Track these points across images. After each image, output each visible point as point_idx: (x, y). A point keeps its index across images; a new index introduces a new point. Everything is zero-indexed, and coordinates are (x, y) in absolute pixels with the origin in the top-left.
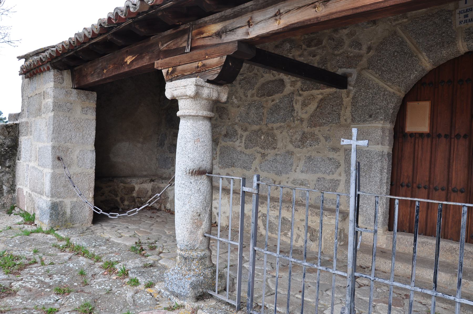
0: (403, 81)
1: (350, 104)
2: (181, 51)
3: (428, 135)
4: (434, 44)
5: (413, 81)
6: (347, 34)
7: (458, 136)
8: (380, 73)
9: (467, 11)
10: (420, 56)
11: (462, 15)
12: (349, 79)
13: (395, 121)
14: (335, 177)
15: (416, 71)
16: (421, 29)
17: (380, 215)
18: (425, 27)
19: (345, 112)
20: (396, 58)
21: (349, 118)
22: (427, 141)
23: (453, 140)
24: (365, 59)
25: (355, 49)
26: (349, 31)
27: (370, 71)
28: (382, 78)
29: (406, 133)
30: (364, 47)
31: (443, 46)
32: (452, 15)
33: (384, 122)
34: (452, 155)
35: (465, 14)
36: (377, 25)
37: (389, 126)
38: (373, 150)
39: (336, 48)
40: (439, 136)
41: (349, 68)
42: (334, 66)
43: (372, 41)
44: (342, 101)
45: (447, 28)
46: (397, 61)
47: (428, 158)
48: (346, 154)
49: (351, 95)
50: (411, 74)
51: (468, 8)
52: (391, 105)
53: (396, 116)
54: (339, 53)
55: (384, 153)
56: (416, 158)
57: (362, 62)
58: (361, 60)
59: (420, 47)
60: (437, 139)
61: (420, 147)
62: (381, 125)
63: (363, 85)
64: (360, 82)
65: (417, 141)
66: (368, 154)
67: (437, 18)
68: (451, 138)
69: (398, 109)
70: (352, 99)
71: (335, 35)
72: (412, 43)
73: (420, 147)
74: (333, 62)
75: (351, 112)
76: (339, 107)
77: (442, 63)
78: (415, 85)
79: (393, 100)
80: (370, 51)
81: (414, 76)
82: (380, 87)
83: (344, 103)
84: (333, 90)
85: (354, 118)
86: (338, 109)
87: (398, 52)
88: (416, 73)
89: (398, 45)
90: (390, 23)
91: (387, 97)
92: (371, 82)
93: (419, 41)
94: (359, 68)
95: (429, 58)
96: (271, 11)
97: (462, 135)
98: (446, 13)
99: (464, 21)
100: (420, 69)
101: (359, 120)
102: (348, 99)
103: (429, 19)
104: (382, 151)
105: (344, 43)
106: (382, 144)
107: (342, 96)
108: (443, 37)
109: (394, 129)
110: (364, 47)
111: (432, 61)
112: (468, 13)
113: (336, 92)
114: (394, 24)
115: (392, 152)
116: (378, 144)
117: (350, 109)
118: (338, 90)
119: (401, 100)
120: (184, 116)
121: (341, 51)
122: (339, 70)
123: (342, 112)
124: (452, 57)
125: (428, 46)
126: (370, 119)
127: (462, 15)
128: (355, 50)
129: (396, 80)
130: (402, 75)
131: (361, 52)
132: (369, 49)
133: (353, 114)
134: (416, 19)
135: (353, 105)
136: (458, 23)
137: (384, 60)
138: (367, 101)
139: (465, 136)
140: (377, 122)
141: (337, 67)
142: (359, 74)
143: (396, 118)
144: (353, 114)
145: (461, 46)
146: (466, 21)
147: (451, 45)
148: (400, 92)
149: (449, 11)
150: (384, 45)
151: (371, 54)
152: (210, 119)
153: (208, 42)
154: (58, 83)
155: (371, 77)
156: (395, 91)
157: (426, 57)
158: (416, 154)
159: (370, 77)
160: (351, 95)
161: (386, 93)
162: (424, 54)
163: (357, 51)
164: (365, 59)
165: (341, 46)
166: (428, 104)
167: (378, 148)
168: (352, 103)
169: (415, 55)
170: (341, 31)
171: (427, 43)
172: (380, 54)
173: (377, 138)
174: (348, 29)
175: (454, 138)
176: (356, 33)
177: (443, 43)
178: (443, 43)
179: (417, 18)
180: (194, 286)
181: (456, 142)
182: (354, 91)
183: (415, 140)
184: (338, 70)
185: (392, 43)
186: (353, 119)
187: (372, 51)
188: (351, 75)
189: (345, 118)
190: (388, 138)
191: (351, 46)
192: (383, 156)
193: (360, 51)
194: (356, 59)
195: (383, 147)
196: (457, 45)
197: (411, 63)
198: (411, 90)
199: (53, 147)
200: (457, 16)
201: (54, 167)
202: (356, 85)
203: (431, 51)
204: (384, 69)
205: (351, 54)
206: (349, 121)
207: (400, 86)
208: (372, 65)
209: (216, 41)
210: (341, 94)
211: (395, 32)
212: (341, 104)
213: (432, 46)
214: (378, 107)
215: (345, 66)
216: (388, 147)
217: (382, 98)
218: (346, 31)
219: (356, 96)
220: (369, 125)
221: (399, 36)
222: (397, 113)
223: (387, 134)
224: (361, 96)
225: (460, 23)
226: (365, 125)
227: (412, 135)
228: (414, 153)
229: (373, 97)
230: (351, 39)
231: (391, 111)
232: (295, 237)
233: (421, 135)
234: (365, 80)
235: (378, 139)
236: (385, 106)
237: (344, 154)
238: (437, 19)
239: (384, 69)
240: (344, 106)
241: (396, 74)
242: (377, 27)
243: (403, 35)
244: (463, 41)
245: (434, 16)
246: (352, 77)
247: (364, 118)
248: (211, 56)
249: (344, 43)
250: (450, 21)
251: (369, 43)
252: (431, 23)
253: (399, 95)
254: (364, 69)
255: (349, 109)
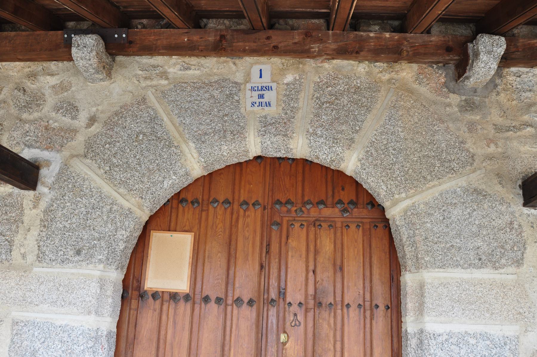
0: (149, 188)
1: (38, 222)
3: (187, 297)
4: (210, 131)
5: (167, 191)
6: (53, 87)
7: (238, 301)
8: (108, 168)
9: (262, 89)
10: (184, 147)
11: (256, 94)
12: (43, 172)
13: (127, 265)
15: (175, 174)
16: (190, 101)
17: (136, 9)
18: (196, 100)
19: (25, 238)
20: (140, 144)
21: (32, 252)
22: (184, 308)
23: (229, 308)
24: (81, 138)
25: (65, 116)
26: (59, 82)
27: (88, 161)
28: (109, 177)
29: (146, 291)
30: (83, 117)
31: (225, 137)
32: (240, 90)
33: (104, 268)
34: (227, 338)
35: (260, 93)
36: (112, 81)
38: (76, 325)
39: (27, 107)
40: (206, 299)
41: (47, 149)
42: (15, 142)
43: (100, 108)
44: (22, 214)
45: (232, 109)
46: (141, 151)
47: (186, 343)
48: (15, 332)
49: (43, 205)
50: (164, 178)
51: (265, 85)
52: (123, 234)
53: (129, 255)
54: (31, 117)
55: (99, 333)
56: (162, 341)
57: (73, 143)
58: (72, 139)
59: (186, 131)
60: (203, 304)
61: (171, 320)
62: (97, 273)
63: (70, 186)
64: (65, 181)
65: (165, 307)
66: (66, 335)
67: (217, 90)
68: (226, 305)
69: (135, 242)
70: (44, 212)
71: (29, 84)
72: (171, 122)
73: (171, 320)
74: (15, 134)
75: (37, 240)
76: (14, 227)
77: (217, 167)
78: (168, 201)
79: (127, 223)
80: (92, 125)
81: (170, 183)
82: (103, 196)
83: (26, 219)
85: (44, 253)
86: (10, 229)
87: (144, 135)
88: (174, 177)
89: (145, 122)
90: (137, 82)
91: (115, 217)
92: (87, 183)
93: (184, 122)
94: (66, 153)
95: (200, 153)
97: (246, 300)
98: (231, 85)
99: (258, 104)
100: (182, 172)
101: (54, 258)
102: (34, 211)
103: (204, 88)
104: (95, 328)
105: (44, 101)
106: (97, 313)
107: (22, 204)
108: (225, 122)
109: (124, 281)
110: (83, 117)
111: (203, 160)
112: (263, 92)
113: (10, 195)
114: (143, 84)
115: (115, 330)
116: (89, 313)
117: (36, 233)
118: (16, 190)
119: (142, 227)
121: (36, 115)
122: (26, 150)
123: (18, 239)
124: (235, 161)
125: (200, 132)
126: (77, 258)
127: (256, 94)
128: (64, 118)
129: (137, 186)
130: (148, 177)
131: (76, 123)
132: (92, 120)
133: (41, 243)
134: (183, 85)
135: (45, 226)
136: (249, 104)
137: (118, 144)
138: (74, 220)
139: (251, 302)
140: (90, 266)
141: (21, 144)
142: (66, 166)
143: (128, 261)
144: (41, 243)
145: (252, 142)
146: (261, 104)
147: (238, 138)
148: (143, 210)
149: (236, 83)
150: (121, 117)
151: (95, 128)
155: (89, 173)
156: (132, 207)
157: (195, 151)
158: (163, 333)
159: (87, 174)
160: (43, 205)
161: (115, 208)
162: (192, 145)
163: (67, 120)
164: (81, 138)
165: (38, 105)
166: (190, 239)
168: (41, 220)
169: (176, 144)
170: (42, 78)
171: (197, 128)
172: (111, 133)
173: (87, 299)
174: (57, 77)
175: (232, 305)
176: (71, 87)
177: (225, 131)
178: (225, 131)
179: (185, 83)
181: (235, 312)
182: (50, 196)
183: (162, 305)
184: (23, 149)
185: (137, 116)
186: (41, 255)
187: (96, 124)
188: (48, 163)
189: (23, 251)
190: (110, 300)
191: (57, 109)
192: (97, 339)
193: (73, 121)
194: (62, 134)
195: (99, 319)
196: (247, 139)
197: (167, 158)
198: (161, 209)
200: (248, 93)
202: (56, 186)
203: (203, 142)
204: (115, 161)
205: (56, 124)
206: (31, 258)
207: (142, 198)
208: (92, 151)
210: (22, 199)
211: (144, 100)
212: (18, 221)
213: (206, 134)
214: (97, 235)
215: (38, 144)
216: (109, 319)
217: (105, 218)
218: (53, 81)
219: (52, 208)
220: (74, 271)
221: (149, 107)
222: (131, 251)
223: (109, 293)
224: (64, 208)
225: (253, 104)
226: (64, 270)
227: (155, 295)
228: (159, 332)
229: (88, 213)
230: (60, 96)
231: (122, 246)
233: (174, 296)
234: (76, 178)
235: (90, 301)
236: (110, 234)
237: (10, 332)
238: (217, 92)
239: (115, 161)
240: (25, 224)
241: (137, 174)
242: (113, 85)
243: (157, 106)
244: (256, 134)
245: (212, 86)
246: (51, 168)
247: (64, 255)
249: (44, 101)
250: (236, 98)
251: (94, 109)
252: (207, 95)
253: (139, 216)
254: (77, 156)
255: (34, 233)
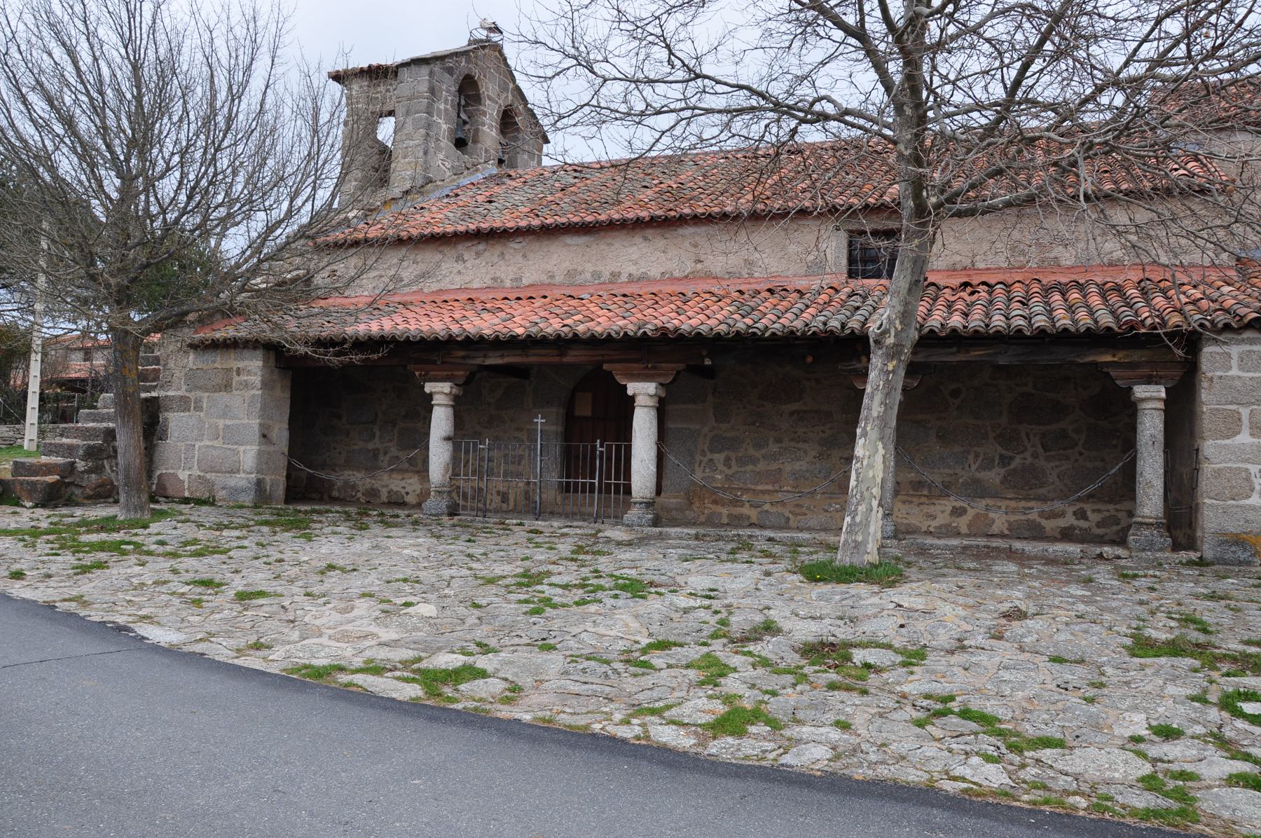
2: (434, 363)
14: (521, 452)
37: (562, 411)
84: (517, 380)
96: (499, 353)
120: (439, 405)
152: (452, 406)
153: (452, 360)
154: (266, 361)
167: (554, 428)
180: (448, 507)
199: (260, 424)
201: (260, 444)
209: (461, 361)
232: (488, 502)
248: (459, 370)
